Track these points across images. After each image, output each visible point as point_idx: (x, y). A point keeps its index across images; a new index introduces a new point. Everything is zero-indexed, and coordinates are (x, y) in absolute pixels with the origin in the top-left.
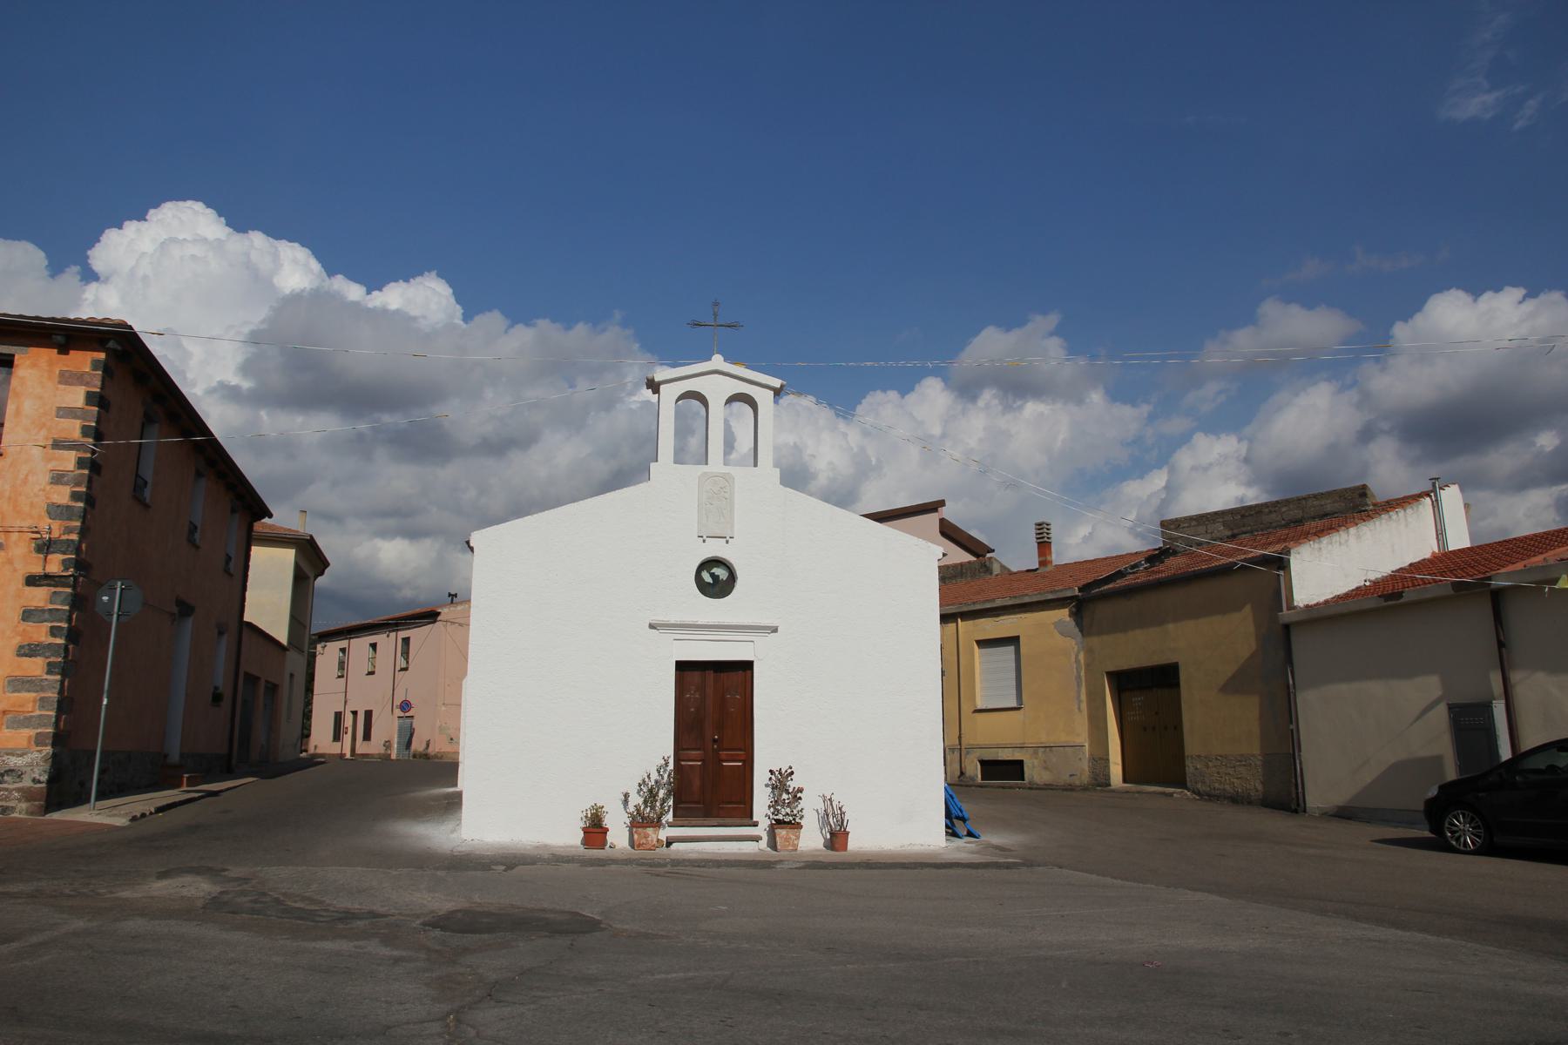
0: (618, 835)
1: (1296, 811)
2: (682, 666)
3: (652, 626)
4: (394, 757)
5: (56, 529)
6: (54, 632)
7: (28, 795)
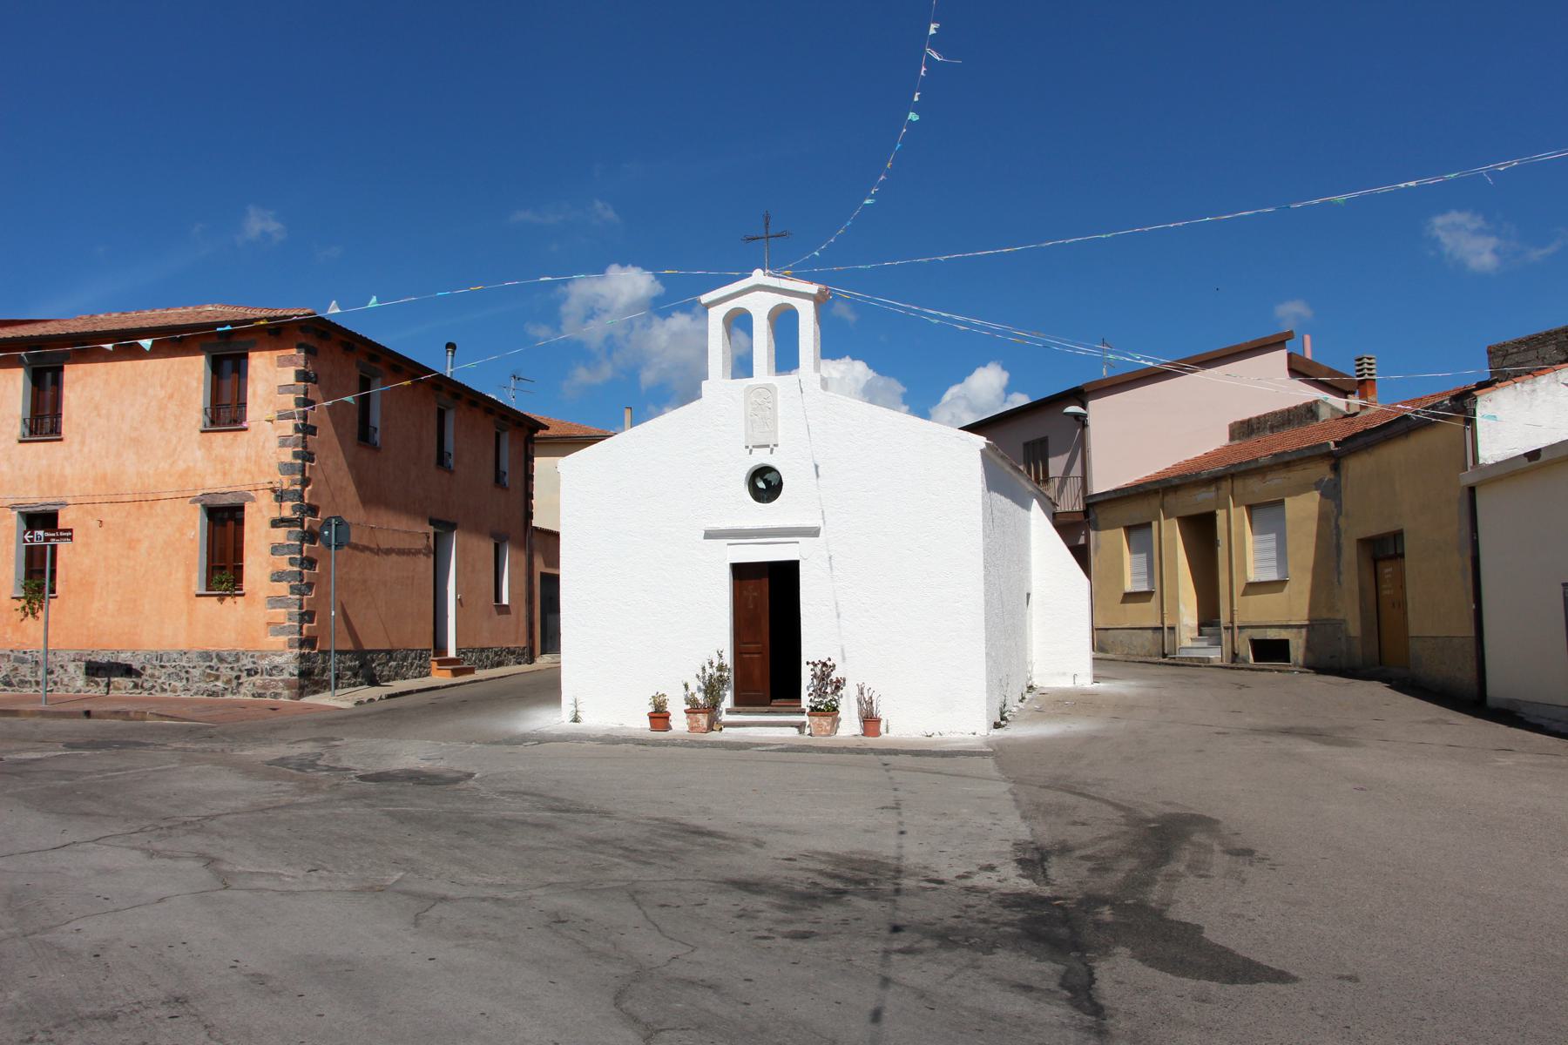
0: (679, 723)
2: (741, 572)
5: (285, 482)
6: (292, 562)
7: (288, 685)
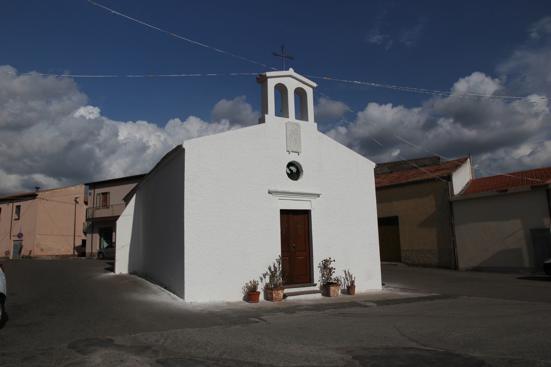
1: (456, 269)
3: (270, 192)
4: (11, 257)
